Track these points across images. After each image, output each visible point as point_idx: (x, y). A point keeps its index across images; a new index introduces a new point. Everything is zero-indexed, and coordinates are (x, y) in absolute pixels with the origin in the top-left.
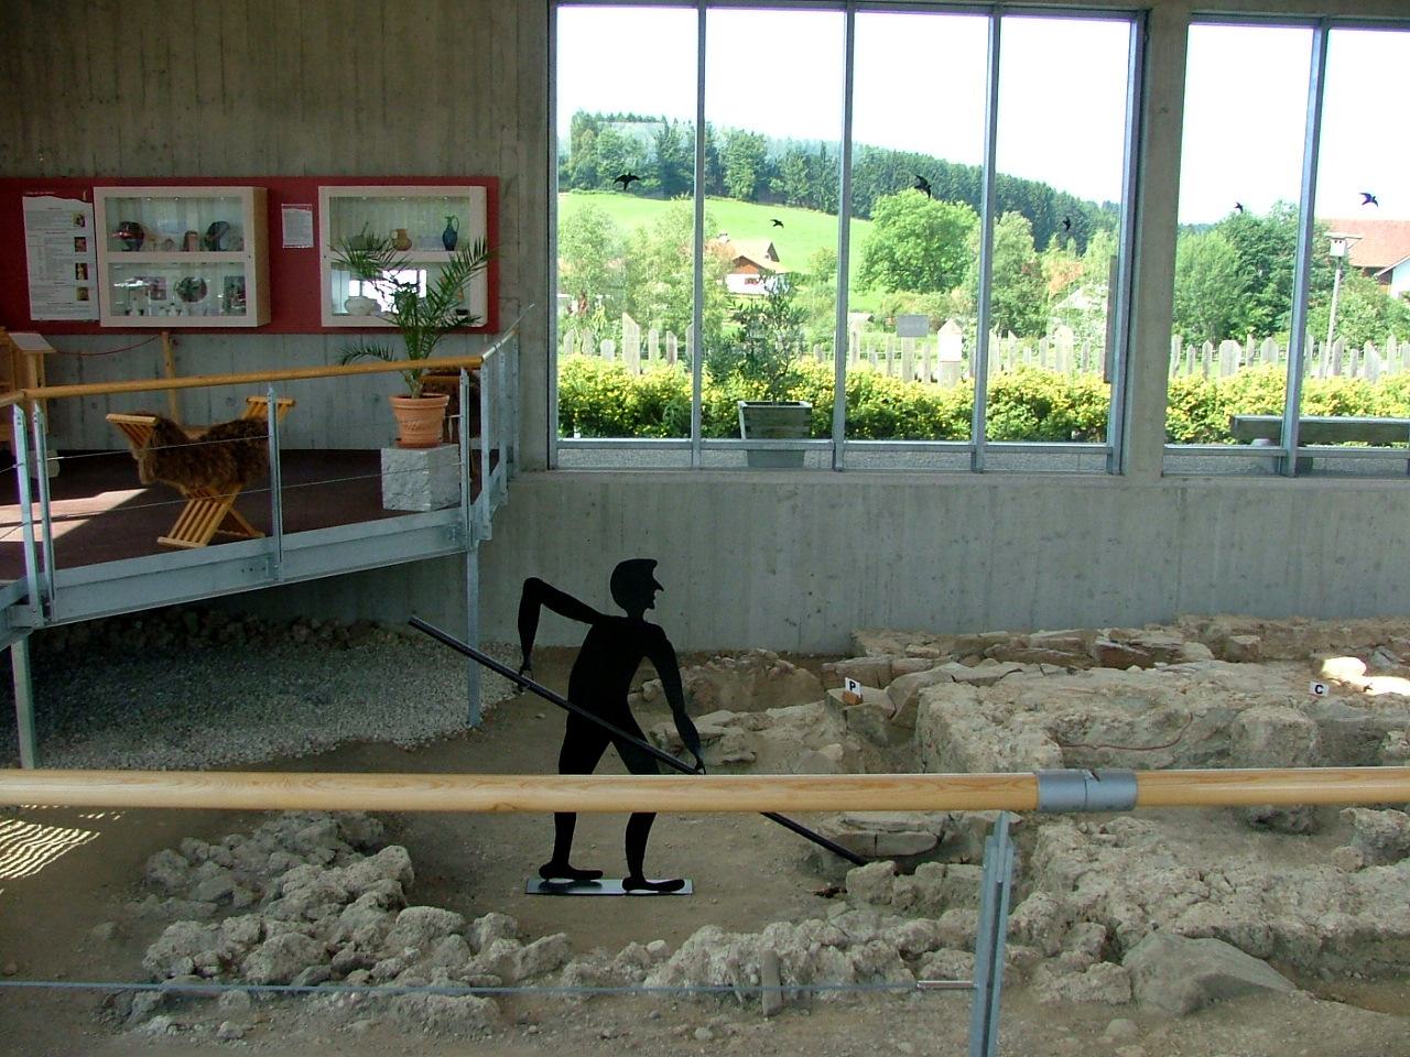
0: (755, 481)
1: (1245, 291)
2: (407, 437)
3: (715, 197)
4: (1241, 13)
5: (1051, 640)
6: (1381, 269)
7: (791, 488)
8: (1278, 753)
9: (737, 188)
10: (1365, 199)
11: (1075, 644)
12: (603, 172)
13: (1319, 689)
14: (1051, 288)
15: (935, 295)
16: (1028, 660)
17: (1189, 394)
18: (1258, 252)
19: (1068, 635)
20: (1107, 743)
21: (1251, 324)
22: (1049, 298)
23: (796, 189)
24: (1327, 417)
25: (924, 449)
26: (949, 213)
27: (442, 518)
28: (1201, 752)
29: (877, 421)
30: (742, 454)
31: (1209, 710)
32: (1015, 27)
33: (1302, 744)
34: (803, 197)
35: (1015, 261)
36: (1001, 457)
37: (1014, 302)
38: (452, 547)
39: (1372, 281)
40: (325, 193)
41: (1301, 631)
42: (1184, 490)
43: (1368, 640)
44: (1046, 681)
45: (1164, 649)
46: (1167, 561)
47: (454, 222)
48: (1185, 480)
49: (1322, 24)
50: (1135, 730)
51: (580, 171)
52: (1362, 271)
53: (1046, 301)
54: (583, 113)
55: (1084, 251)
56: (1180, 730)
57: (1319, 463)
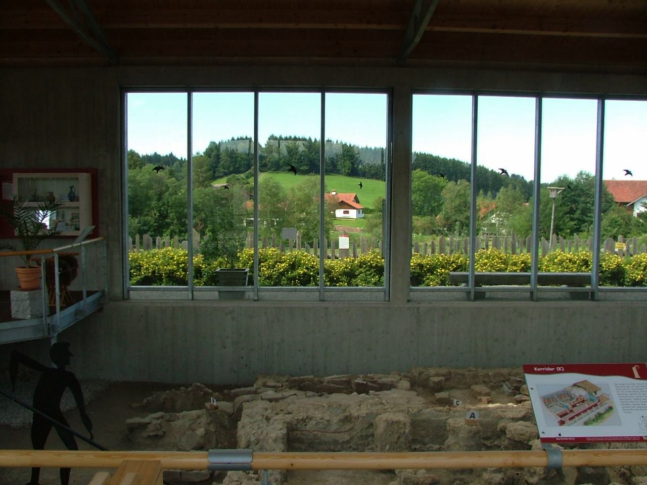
0: (215, 305)
1: (566, 214)
2: (23, 286)
3: (333, 174)
4: (236, 86)
5: (334, 380)
6: (628, 203)
7: (231, 309)
8: (390, 435)
9: (343, 170)
10: (626, 173)
11: (346, 381)
12: (282, 163)
13: (458, 403)
14: (481, 214)
15: (428, 218)
16: (300, 389)
17: (453, 262)
18: (571, 196)
19: (343, 377)
20: (316, 430)
21: (568, 229)
22: (480, 218)
23: (370, 170)
24: (519, 273)
25: (295, 290)
26: (435, 180)
27: (35, 322)
28: (364, 434)
29: (302, 277)
30: (217, 293)
31: (367, 414)
32: (199, 97)
33: (402, 431)
34: (373, 174)
35: (464, 202)
36: (609, 294)
37: (464, 220)
38: (41, 336)
39: (622, 208)
40: (16, 176)
41: (469, 374)
42: (418, 308)
43: (502, 379)
44: (306, 400)
45: (387, 384)
46: (411, 342)
47: (73, 190)
48: (419, 303)
49: (475, 93)
50: (331, 424)
51: (272, 163)
52: (619, 204)
53: (478, 220)
54: (273, 136)
55: (495, 197)
56: (353, 424)
57: (488, 295)
